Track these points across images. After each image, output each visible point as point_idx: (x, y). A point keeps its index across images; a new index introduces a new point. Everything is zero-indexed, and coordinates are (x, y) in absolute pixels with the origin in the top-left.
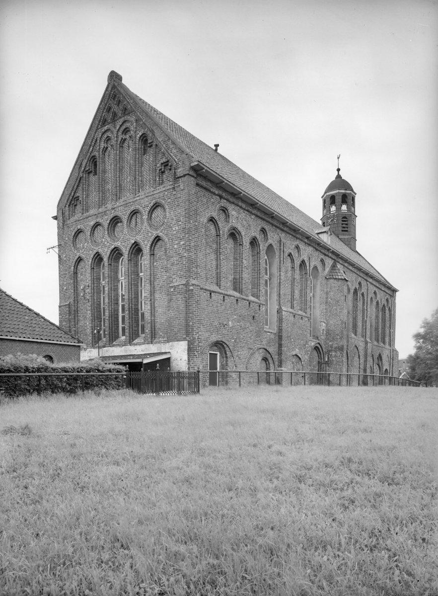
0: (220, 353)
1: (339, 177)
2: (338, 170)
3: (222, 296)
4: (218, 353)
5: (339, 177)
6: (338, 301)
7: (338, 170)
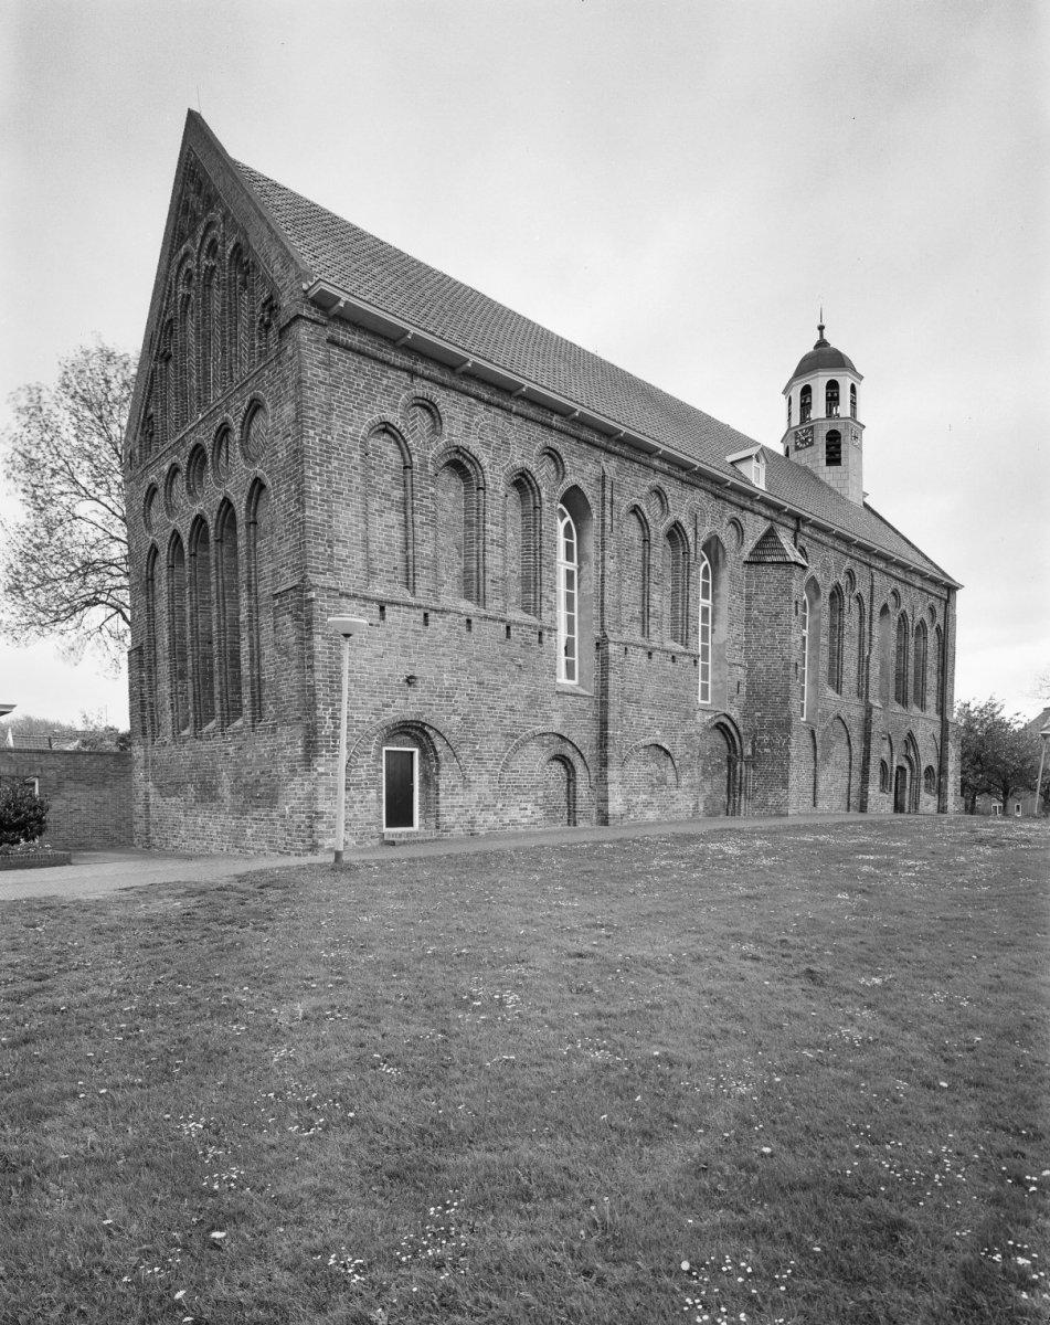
0: (424, 753)
1: (822, 343)
2: (821, 328)
3: (421, 612)
4: (417, 751)
5: (822, 343)
6: (777, 615)
7: (821, 328)
